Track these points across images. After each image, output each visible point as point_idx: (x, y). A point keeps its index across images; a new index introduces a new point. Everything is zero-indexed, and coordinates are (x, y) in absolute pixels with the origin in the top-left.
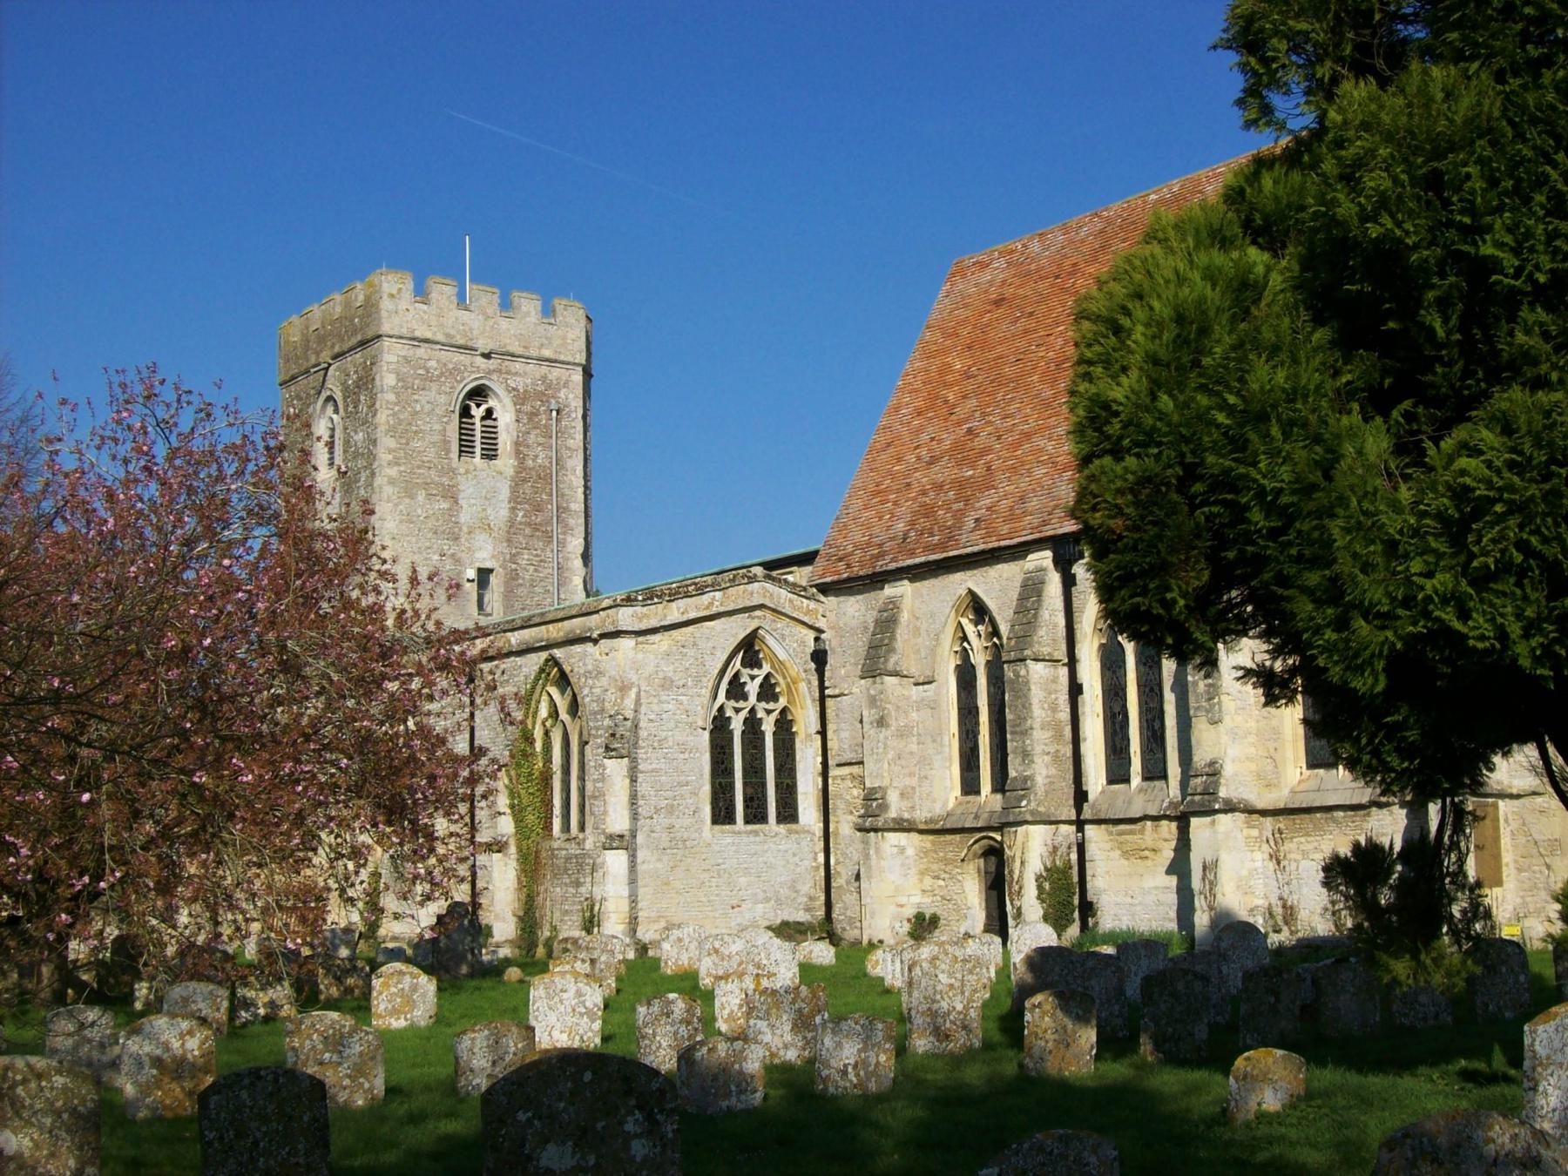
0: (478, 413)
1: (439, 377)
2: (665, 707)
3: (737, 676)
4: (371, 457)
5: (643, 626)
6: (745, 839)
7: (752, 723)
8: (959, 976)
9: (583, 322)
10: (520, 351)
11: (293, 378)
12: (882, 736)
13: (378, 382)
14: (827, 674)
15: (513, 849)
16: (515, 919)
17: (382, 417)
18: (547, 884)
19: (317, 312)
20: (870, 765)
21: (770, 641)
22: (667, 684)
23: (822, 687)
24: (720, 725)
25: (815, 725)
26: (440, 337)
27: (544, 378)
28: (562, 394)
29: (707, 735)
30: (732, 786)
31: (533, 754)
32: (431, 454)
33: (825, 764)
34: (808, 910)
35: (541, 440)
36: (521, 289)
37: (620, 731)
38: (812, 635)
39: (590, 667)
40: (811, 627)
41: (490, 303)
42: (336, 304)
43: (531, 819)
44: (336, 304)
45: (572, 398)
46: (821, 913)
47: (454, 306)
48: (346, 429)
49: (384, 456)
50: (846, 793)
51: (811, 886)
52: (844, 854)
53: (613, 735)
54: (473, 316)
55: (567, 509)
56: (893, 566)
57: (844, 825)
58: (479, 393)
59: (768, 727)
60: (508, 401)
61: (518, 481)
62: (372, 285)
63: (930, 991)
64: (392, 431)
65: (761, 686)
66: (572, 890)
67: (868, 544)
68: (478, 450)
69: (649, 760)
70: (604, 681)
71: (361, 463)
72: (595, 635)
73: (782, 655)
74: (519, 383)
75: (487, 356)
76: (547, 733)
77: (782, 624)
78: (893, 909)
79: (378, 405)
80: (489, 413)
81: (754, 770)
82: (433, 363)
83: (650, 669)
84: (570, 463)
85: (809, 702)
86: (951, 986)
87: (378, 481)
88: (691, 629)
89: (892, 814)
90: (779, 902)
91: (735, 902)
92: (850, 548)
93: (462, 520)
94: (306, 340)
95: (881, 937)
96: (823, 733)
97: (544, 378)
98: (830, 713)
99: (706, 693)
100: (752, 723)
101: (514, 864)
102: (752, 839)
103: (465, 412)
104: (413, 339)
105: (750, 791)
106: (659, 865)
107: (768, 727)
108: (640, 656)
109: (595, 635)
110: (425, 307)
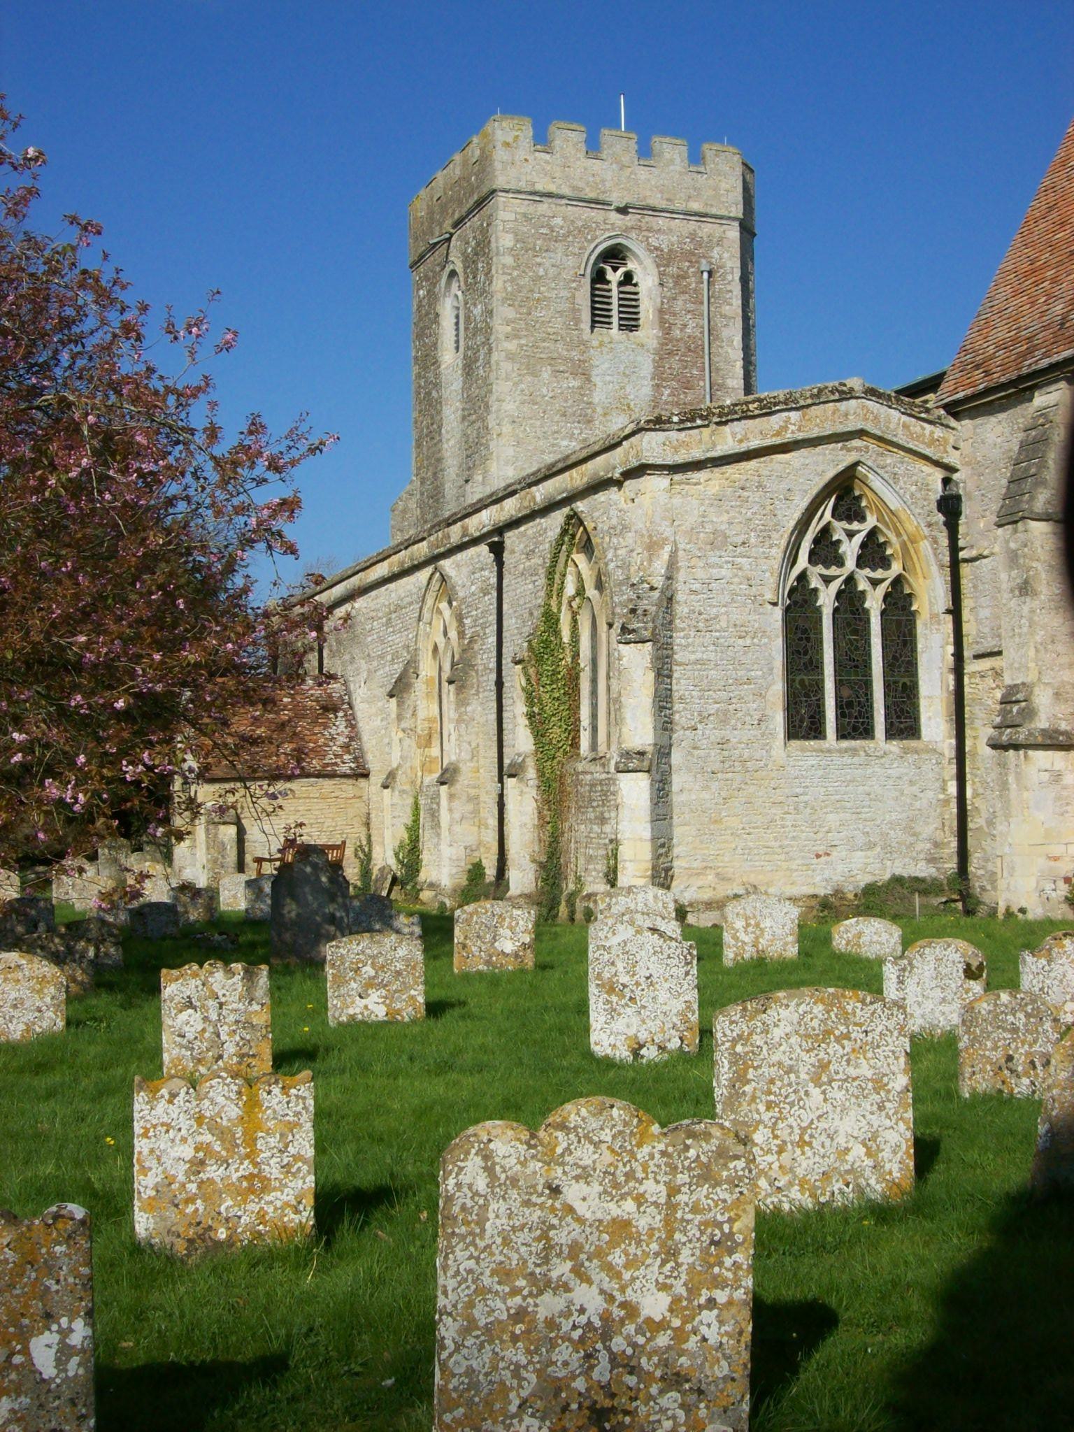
0: (614, 277)
1: (566, 236)
2: (715, 572)
3: (826, 531)
4: (488, 330)
5: (680, 459)
6: (837, 760)
7: (850, 598)
8: (654, 1189)
9: (739, 169)
10: (663, 204)
11: (422, 257)
12: (1026, 609)
13: (493, 245)
14: (962, 529)
15: (531, 773)
16: (534, 866)
17: (498, 284)
18: (572, 820)
19: (441, 177)
20: (1010, 654)
21: (875, 482)
22: (718, 541)
23: (954, 548)
24: (799, 603)
25: (942, 599)
26: (566, 191)
27: (692, 236)
28: (715, 253)
29: (778, 613)
30: (819, 687)
31: (560, 644)
32: (558, 324)
33: (959, 656)
34: (932, 860)
35: (690, 306)
36: (665, 133)
37: (644, 604)
38: (939, 475)
39: (614, 521)
40: (937, 464)
41: (627, 150)
42: (455, 169)
43: (557, 733)
44: (455, 169)
45: (729, 258)
46: (951, 865)
47: (582, 155)
48: (466, 303)
49: (500, 329)
50: (984, 696)
51: (937, 826)
52: (984, 783)
53: (633, 611)
54: (605, 165)
55: (722, 386)
56: (1045, 363)
57: (980, 734)
58: (615, 255)
59: (874, 603)
60: (649, 262)
61: (664, 352)
62: (486, 136)
63: (525, 1248)
64: (510, 299)
65: (863, 546)
66: (596, 828)
67: (1015, 341)
68: (615, 320)
69: (688, 648)
70: (630, 537)
71: (480, 339)
72: (617, 475)
73: (894, 503)
74: (663, 242)
75: (623, 210)
76: (575, 621)
77: (892, 459)
78: (1042, 862)
79: (493, 272)
80: (628, 278)
81: (853, 663)
82: (558, 221)
83: (691, 520)
84: (725, 333)
85: (934, 568)
86: (621, 1228)
87: (495, 356)
88: (753, 464)
89: (1042, 722)
90: (888, 849)
91: (821, 849)
92: (991, 350)
93: (596, 400)
94: (431, 213)
95: (1024, 904)
96: (955, 611)
97: (692, 236)
98: (966, 585)
99: (777, 553)
100: (850, 598)
101: (534, 792)
102: (847, 760)
103: (599, 277)
104: (534, 193)
105: (846, 692)
106: (706, 795)
107: (874, 603)
108: (677, 501)
109: (617, 475)
110: (548, 157)
